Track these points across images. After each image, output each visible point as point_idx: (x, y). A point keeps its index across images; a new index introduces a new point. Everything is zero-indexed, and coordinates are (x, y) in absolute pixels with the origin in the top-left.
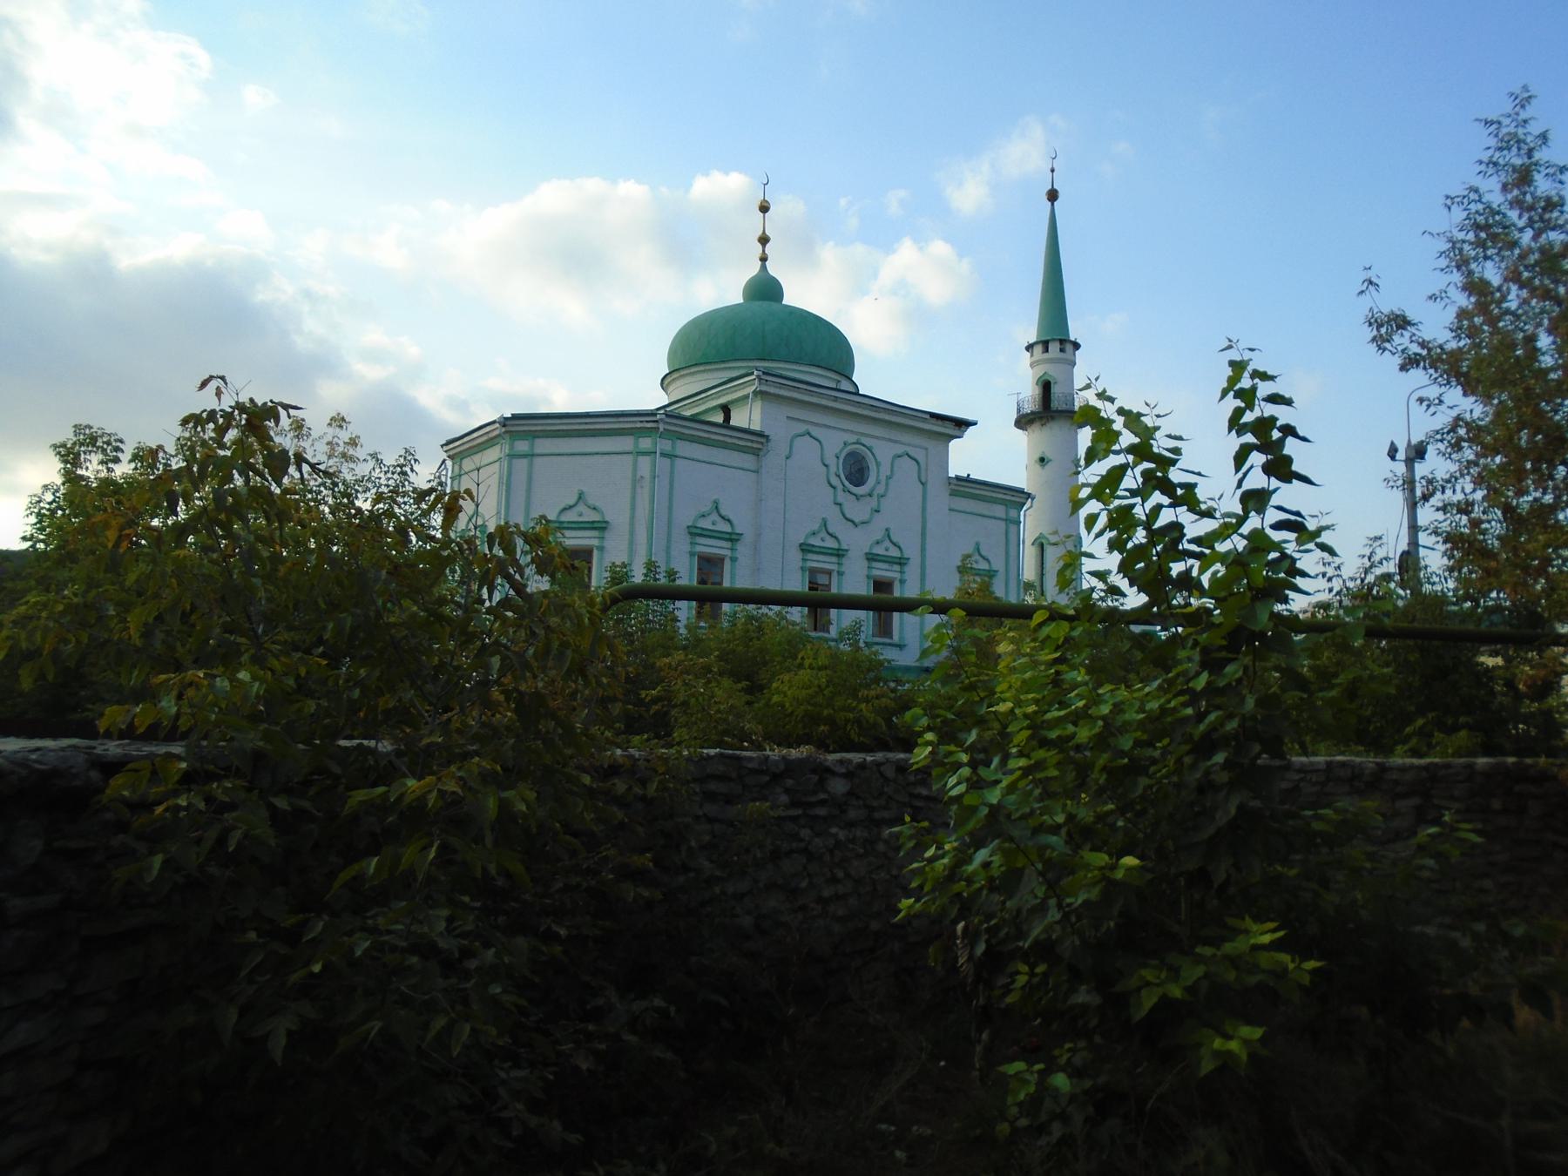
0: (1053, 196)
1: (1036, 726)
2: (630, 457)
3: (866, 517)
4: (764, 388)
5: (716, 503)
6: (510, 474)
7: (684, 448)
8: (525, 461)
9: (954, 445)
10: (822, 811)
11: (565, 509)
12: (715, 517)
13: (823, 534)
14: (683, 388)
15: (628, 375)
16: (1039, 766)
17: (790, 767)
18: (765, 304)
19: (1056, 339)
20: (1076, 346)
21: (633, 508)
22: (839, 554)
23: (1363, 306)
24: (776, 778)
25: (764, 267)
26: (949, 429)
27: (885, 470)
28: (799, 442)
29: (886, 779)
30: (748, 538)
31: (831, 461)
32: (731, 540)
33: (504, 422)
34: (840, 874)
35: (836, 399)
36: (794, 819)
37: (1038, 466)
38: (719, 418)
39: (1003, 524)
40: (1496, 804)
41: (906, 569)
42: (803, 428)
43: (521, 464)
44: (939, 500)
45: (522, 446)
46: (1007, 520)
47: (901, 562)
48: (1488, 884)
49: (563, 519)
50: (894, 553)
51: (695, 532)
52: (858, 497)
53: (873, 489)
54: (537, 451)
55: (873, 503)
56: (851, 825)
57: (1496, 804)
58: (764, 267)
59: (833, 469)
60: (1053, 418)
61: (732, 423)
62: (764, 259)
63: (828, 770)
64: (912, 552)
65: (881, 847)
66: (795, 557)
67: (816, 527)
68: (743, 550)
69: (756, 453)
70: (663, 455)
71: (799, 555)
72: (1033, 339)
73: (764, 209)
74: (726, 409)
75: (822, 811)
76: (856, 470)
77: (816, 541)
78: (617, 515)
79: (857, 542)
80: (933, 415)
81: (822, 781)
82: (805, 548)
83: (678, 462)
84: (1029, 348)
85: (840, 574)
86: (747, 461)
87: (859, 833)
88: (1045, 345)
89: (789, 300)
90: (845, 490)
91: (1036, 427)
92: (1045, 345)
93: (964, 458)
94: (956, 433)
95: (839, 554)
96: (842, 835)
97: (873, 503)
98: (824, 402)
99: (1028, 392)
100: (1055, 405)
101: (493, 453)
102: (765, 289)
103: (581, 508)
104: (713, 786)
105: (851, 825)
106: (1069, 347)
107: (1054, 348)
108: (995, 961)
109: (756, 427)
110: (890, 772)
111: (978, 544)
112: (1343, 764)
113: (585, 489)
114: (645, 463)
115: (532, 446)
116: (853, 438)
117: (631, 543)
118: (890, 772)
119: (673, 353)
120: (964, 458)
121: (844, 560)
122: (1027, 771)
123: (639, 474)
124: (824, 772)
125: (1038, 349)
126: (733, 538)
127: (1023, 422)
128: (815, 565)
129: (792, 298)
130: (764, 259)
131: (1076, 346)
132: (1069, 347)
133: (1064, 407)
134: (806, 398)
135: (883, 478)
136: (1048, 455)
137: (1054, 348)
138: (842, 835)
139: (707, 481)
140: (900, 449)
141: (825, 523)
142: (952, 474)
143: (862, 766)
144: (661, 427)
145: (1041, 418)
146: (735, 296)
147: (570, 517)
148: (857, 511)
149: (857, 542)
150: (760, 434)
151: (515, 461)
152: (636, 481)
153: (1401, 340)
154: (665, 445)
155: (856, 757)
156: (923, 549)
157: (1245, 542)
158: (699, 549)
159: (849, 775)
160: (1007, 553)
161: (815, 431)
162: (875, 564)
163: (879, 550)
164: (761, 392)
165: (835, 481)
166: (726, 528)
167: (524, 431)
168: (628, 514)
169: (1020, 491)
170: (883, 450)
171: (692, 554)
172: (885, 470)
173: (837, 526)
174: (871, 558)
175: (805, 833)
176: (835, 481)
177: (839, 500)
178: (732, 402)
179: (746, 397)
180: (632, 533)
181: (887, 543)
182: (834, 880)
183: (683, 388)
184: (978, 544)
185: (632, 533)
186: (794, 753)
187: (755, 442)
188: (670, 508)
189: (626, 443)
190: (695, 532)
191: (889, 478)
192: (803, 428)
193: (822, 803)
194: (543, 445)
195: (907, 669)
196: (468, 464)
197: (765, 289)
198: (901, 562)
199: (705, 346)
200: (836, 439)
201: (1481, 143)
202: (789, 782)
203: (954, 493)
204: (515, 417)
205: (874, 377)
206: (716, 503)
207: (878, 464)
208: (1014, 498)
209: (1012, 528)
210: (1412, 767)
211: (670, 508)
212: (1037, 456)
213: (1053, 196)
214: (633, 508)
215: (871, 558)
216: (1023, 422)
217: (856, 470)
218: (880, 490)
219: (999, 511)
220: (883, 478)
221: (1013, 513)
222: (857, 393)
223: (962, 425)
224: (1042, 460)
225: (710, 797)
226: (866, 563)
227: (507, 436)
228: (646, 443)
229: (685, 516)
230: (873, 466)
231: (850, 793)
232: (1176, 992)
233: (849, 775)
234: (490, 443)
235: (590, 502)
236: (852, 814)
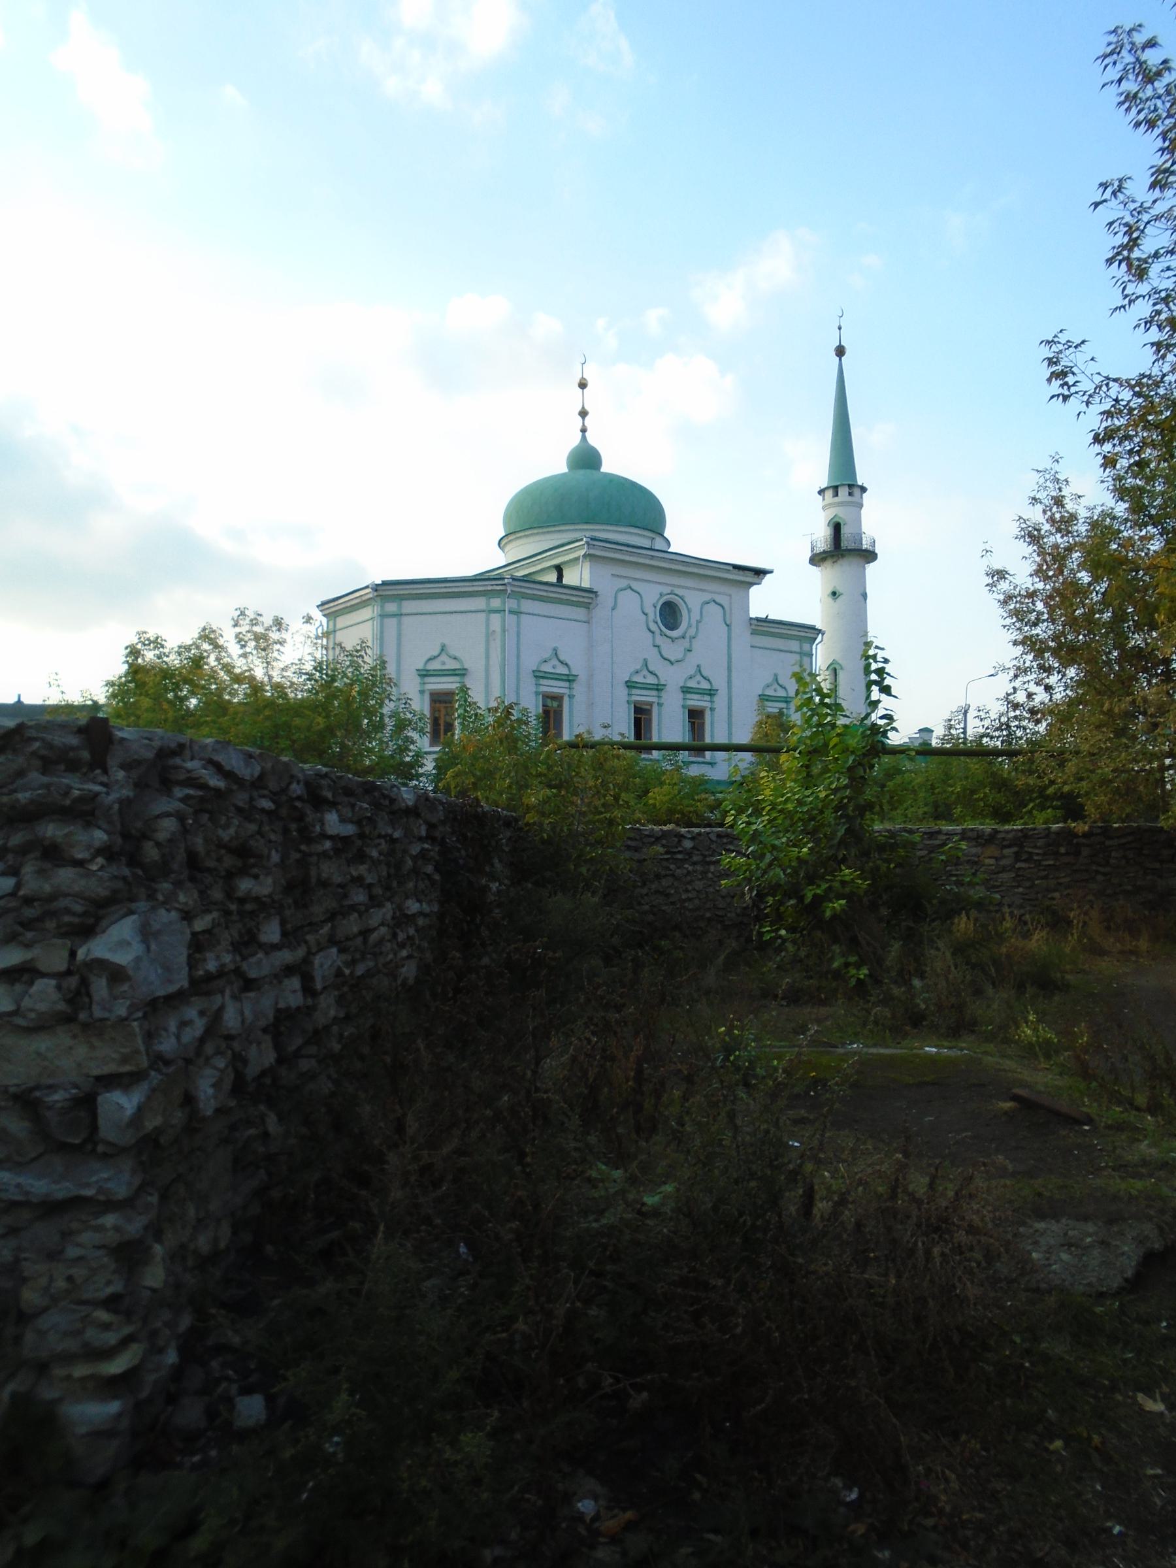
1: (774, 806)
2: (482, 616)
3: (680, 656)
4: (592, 552)
5: (555, 650)
6: (382, 632)
7: (527, 605)
8: (394, 620)
9: (754, 590)
10: (680, 856)
12: (555, 662)
13: (645, 672)
14: (522, 548)
15: (471, 544)
16: (775, 819)
17: (665, 834)
18: (588, 471)
19: (844, 484)
20: (863, 489)
21: (487, 657)
22: (659, 688)
23: (983, 565)
24: (658, 839)
25: (584, 438)
26: (749, 577)
27: (695, 616)
29: (712, 841)
30: (583, 677)
31: (649, 610)
32: (569, 681)
33: (376, 588)
34: (690, 888)
36: (667, 859)
37: (830, 600)
38: (552, 577)
39: (797, 657)
40: (1062, 850)
41: (716, 699)
42: (624, 583)
43: (391, 623)
44: (742, 638)
45: (391, 607)
46: (802, 654)
47: (711, 693)
48: (1057, 895)
50: (705, 685)
51: (539, 675)
52: (673, 640)
56: (694, 864)
57: (1062, 850)
58: (584, 438)
59: (651, 617)
60: (843, 556)
61: (565, 581)
62: (584, 430)
63: (683, 836)
64: (719, 683)
65: (710, 875)
66: (622, 692)
68: (579, 689)
69: (587, 606)
70: (511, 612)
71: (625, 691)
72: (824, 485)
73: (583, 385)
74: (559, 569)
75: (680, 856)
76: (670, 613)
77: (638, 679)
78: (473, 661)
79: (674, 678)
80: (736, 567)
81: (680, 841)
82: (630, 685)
83: (523, 617)
86: (580, 613)
87: (699, 868)
88: (835, 489)
89: (606, 468)
90: (662, 634)
91: (828, 563)
92: (835, 489)
93: (763, 602)
94: (755, 580)
95: (659, 688)
96: (690, 868)
97: (686, 643)
98: (641, 560)
99: (821, 535)
100: (844, 544)
101: (366, 613)
102: (586, 458)
103: (444, 657)
104: (629, 843)
105: (694, 864)
107: (843, 492)
108: (761, 896)
109: (586, 584)
110: (714, 838)
111: (776, 675)
112: (972, 830)
113: (446, 642)
114: (496, 619)
115: (400, 607)
116: (667, 590)
117: (487, 686)
118: (714, 838)
119: (508, 518)
120: (763, 602)
121: (663, 694)
122: (770, 821)
123: (492, 628)
124: (681, 837)
125: (829, 493)
126: (570, 679)
127: (817, 559)
128: (638, 698)
130: (584, 430)
131: (863, 489)
132: (857, 491)
133: (852, 546)
134: (627, 558)
135: (694, 622)
136: (839, 589)
137: (843, 492)
138: (690, 868)
139: (548, 633)
142: (753, 615)
143: (699, 834)
144: (509, 589)
145: (832, 556)
146: (558, 466)
148: (673, 651)
149: (674, 678)
150: (589, 591)
151: (386, 620)
152: (489, 635)
153: (1004, 586)
154: (511, 604)
155: (696, 830)
156: (729, 682)
159: (693, 839)
161: (634, 585)
162: (689, 696)
163: (692, 684)
164: (590, 555)
165: (653, 627)
166: (565, 671)
167: (393, 595)
168: (483, 662)
169: (813, 628)
170: (692, 599)
171: (537, 693)
172: (695, 616)
173: (656, 664)
174: (686, 690)
175: (672, 867)
176: (653, 627)
179: (577, 559)
181: (699, 678)
182: (687, 891)
183: (522, 548)
184: (776, 675)
186: (665, 828)
187: (585, 597)
188: (518, 657)
189: (479, 603)
190: (539, 675)
191: (698, 622)
192: (624, 583)
193: (680, 852)
194: (409, 606)
195: (719, 782)
196: (342, 621)
197: (586, 458)
198: (711, 693)
199: (536, 511)
200: (653, 593)
201: (1030, 483)
202: (664, 842)
203: (754, 633)
204: (384, 583)
205: (686, 536)
206: (555, 650)
207: (689, 611)
208: (808, 633)
209: (806, 660)
210: (1013, 830)
211: (518, 657)
212: (830, 591)
213: (840, 351)
214: (487, 657)
215: (686, 690)
216: (817, 559)
217: (670, 613)
218: (692, 632)
219: (794, 645)
220: (694, 622)
221: (806, 647)
223: (760, 573)
224: (834, 594)
225: (628, 847)
226: (681, 695)
227: (378, 599)
228: (496, 603)
229: (530, 662)
230: (684, 612)
231: (693, 848)
232: (818, 891)
233: (693, 839)
234: (363, 604)
235: (452, 652)
236: (695, 858)
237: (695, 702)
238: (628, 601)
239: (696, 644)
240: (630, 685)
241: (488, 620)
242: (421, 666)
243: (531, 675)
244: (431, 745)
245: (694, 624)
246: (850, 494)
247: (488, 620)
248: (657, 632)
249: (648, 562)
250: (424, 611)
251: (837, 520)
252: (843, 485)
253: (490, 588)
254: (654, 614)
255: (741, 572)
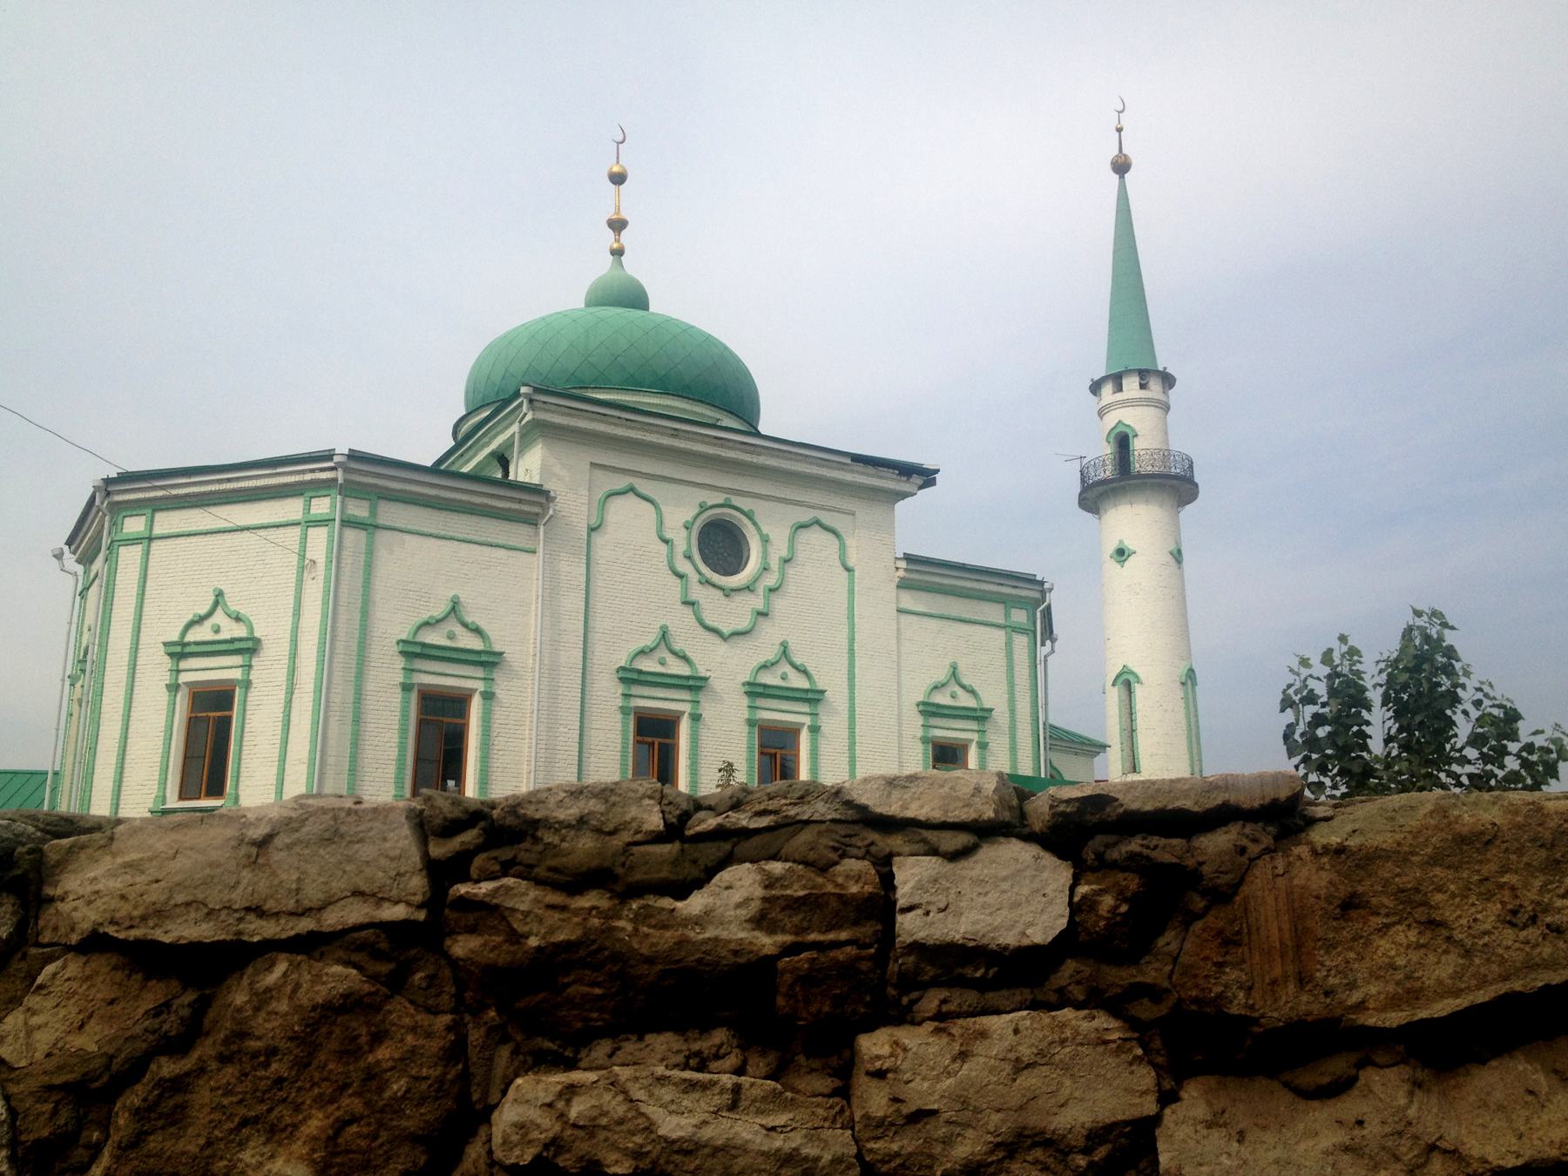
0: (1121, 167)
3: (744, 624)
7: (391, 513)
9: (901, 506)
11: (427, 624)
20: (1168, 380)
21: (297, 613)
26: (891, 483)
27: (779, 549)
28: (804, 536)
30: (836, 693)
35: (675, 433)
42: (621, 482)
47: (813, 697)
49: (190, 638)
53: (756, 580)
54: (157, 531)
55: (757, 602)
62: (618, 253)
64: (831, 680)
67: (649, 640)
74: (502, 460)
76: (721, 544)
79: (728, 668)
80: (858, 459)
83: (383, 536)
84: (1096, 388)
85: (696, 718)
89: (654, 307)
94: (904, 486)
95: (695, 685)
103: (219, 618)
106: (1155, 387)
107: (1131, 385)
116: (719, 498)
123: (309, 555)
129: (660, 304)
134: (620, 432)
137: (1131, 385)
140: (805, 515)
141: (664, 635)
147: (202, 633)
148: (736, 614)
149: (728, 668)
150: (536, 490)
152: (304, 565)
154: (359, 510)
157: (473, 1171)
158: (184, 678)
160: (358, 720)
161: (644, 486)
165: (684, 566)
171: (406, 688)
174: (756, 691)
176: (684, 566)
177: (693, 597)
178: (509, 444)
180: (294, 655)
184: (954, 668)
185: (294, 655)
189: (292, 509)
192: (621, 482)
198: (248, 648)
203: (904, 585)
207: (765, 540)
213: (1121, 167)
214: (297, 613)
215: (756, 691)
217: (721, 544)
218: (771, 580)
220: (774, 564)
222: (758, 435)
223: (927, 477)
228: (321, 506)
235: (234, 607)
237: (949, 731)
238: (630, 519)
239: (779, 604)
240: (930, 711)
241: (304, 538)
242: (174, 636)
243: (615, 676)
244: (181, 798)
245: (774, 564)
246: (1143, 387)
247: (304, 538)
248: (694, 577)
249: (666, 441)
250: (194, 528)
251: (1121, 429)
252: (1128, 372)
253: (308, 477)
254: (683, 541)
255: (870, 470)
